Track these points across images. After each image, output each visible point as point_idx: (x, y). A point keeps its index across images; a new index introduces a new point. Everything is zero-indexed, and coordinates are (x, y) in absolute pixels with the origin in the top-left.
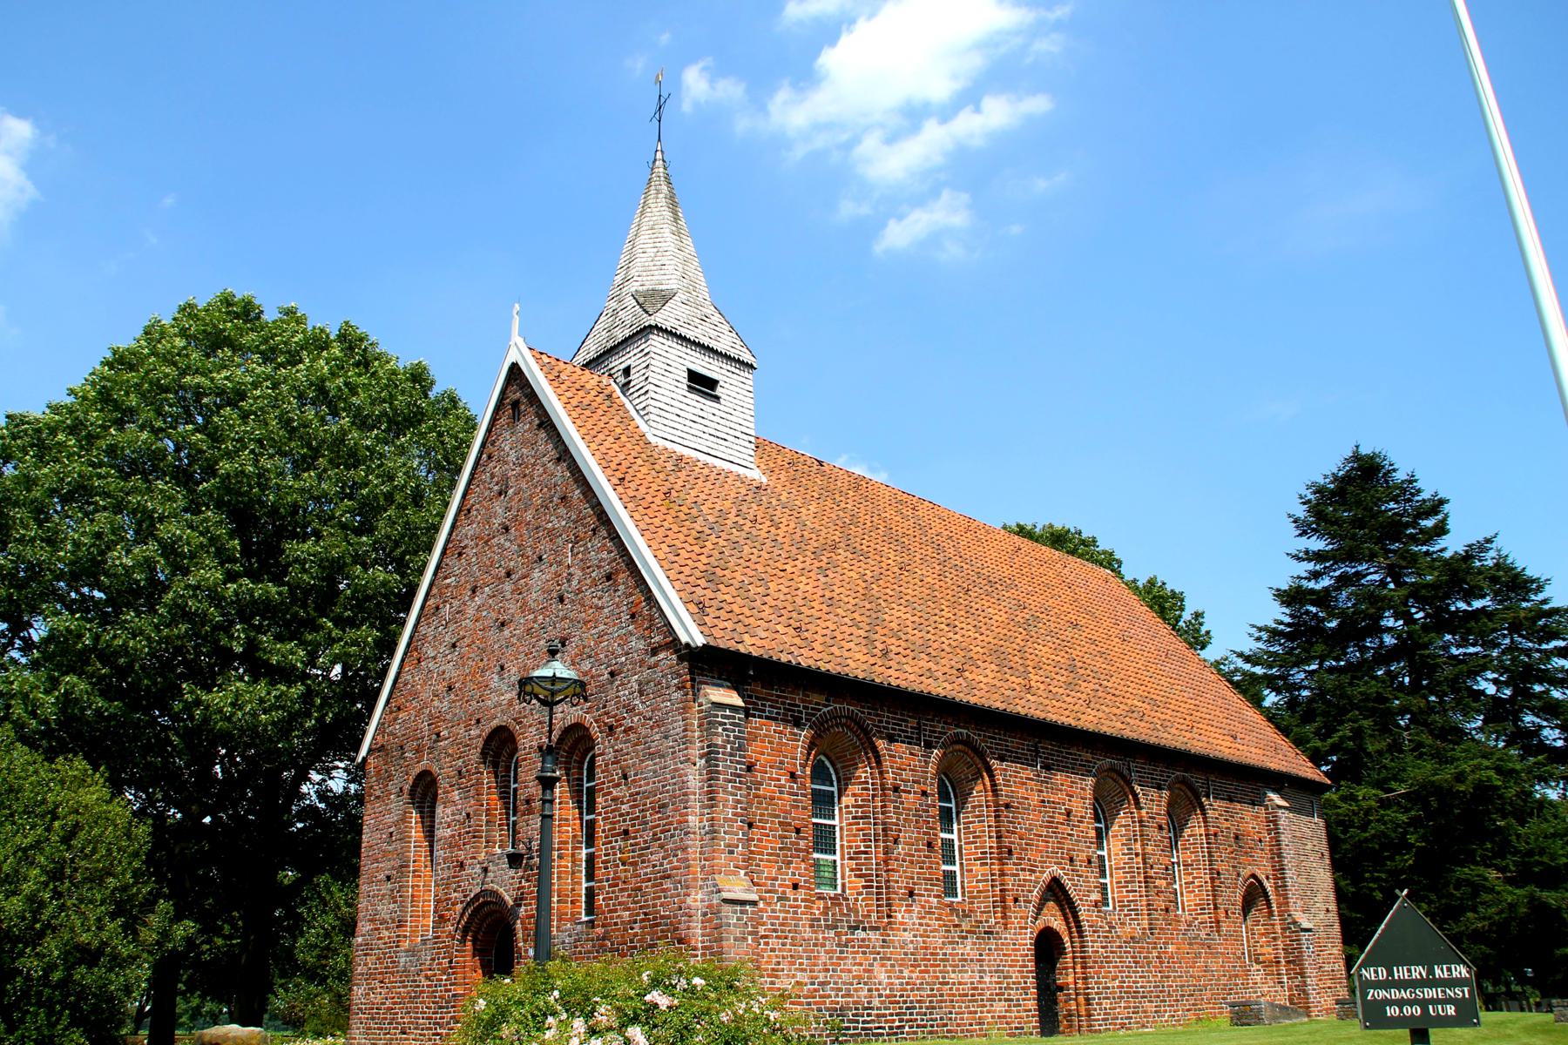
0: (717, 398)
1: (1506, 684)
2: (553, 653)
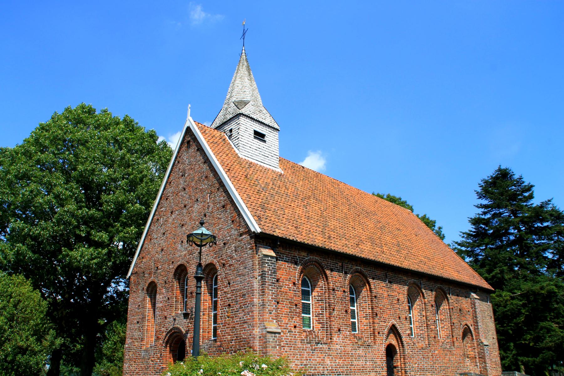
0: (265, 141)
1: (556, 254)
2: (202, 224)
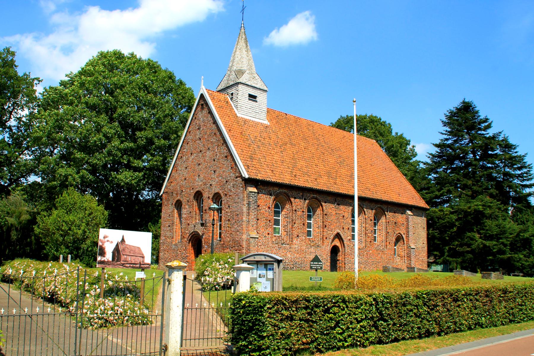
0: (256, 101)
